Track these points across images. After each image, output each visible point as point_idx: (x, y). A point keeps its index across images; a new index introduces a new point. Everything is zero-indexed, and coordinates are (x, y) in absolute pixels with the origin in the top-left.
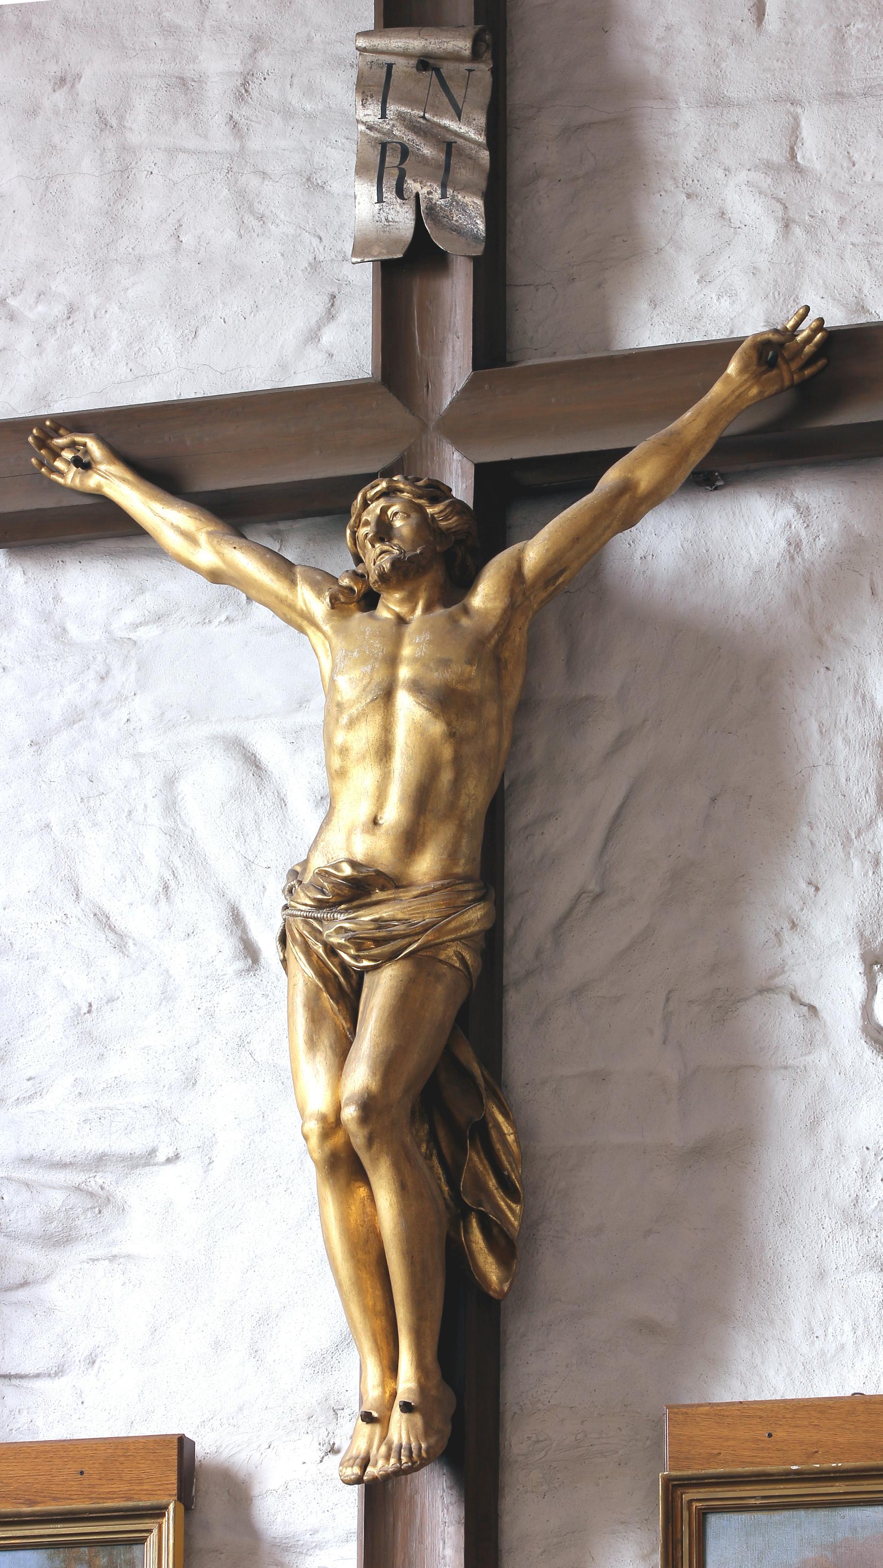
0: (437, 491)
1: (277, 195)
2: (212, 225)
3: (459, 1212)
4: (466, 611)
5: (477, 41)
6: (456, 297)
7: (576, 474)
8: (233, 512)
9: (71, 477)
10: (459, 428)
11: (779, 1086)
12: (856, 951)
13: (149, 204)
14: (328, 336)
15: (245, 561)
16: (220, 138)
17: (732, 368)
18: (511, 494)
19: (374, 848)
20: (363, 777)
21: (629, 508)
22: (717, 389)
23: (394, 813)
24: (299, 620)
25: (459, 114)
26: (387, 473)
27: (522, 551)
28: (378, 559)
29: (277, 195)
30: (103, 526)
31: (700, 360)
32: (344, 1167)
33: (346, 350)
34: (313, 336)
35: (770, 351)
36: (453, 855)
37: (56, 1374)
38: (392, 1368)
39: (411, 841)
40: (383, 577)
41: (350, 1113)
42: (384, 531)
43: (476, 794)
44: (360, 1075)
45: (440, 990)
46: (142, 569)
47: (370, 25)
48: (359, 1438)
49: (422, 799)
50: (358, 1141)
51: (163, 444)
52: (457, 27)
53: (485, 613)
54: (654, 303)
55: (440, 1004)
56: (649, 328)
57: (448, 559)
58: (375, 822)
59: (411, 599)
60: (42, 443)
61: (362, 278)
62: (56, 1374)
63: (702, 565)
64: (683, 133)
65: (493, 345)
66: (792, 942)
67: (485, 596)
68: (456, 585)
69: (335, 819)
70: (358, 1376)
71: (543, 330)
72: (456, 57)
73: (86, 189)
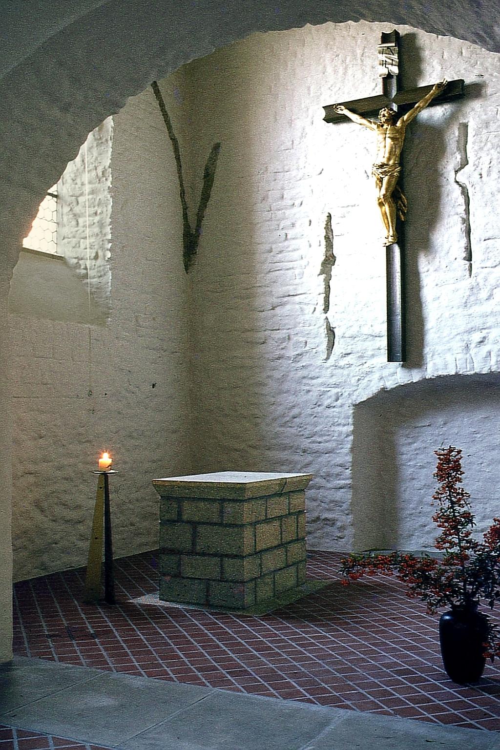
0: (392, 110)
1: (368, 69)
2: (359, 74)
3: (398, 210)
4: (396, 126)
5: (395, 44)
6: (394, 81)
7: (411, 106)
8: (364, 115)
9: (340, 112)
10: (394, 101)
11: (443, 189)
12: (454, 171)
13: (350, 72)
14: (376, 89)
15: (364, 121)
16: (359, 61)
17: (434, 88)
18: (403, 110)
19: (385, 161)
20: (382, 150)
21: (421, 109)
22: (432, 91)
23: (387, 155)
24: (372, 129)
25: (393, 55)
26: (384, 108)
27: (403, 118)
28: (383, 119)
29: (368, 69)
30: (345, 119)
31: (430, 87)
32: (381, 204)
33: (379, 91)
34: (374, 89)
35: (440, 85)
36: (395, 160)
37: (342, 368)
38: (389, 232)
39: (389, 159)
40: (384, 122)
41: (382, 197)
42: (384, 116)
43: (398, 152)
44: (383, 191)
45: (394, 179)
46: (351, 124)
47: (380, 43)
48: (386, 241)
49: (390, 153)
50: (383, 200)
51: (352, 106)
52: (392, 42)
53: (399, 127)
54: (423, 81)
55: (394, 181)
56: (422, 84)
57: (393, 119)
58: (384, 157)
59: (388, 125)
60: (336, 108)
61: (380, 81)
62: (342, 368)
63: (431, 117)
64: (426, 54)
65: (400, 88)
66: (445, 170)
67: (399, 124)
68: (394, 123)
69: (336, 335)
70: (385, 233)
71: (406, 84)
72: (393, 47)
73: (341, 71)
